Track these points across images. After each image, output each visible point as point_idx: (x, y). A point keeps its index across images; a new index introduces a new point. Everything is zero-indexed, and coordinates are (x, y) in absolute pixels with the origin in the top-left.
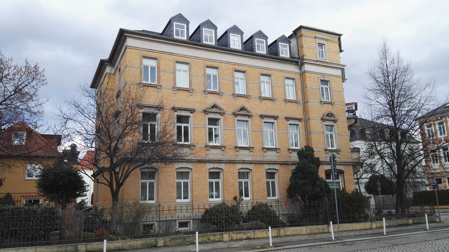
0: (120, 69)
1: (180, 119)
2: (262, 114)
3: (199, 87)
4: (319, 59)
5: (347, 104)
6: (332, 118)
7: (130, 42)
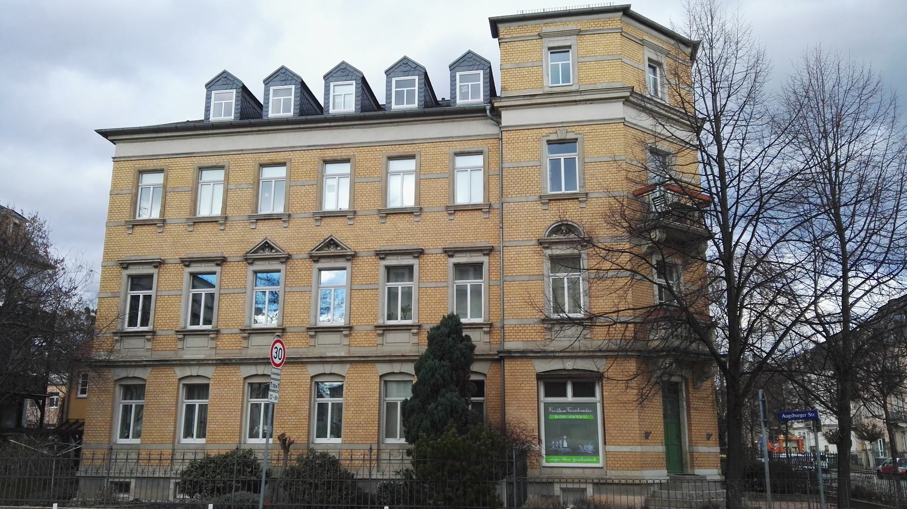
1: (138, 282)
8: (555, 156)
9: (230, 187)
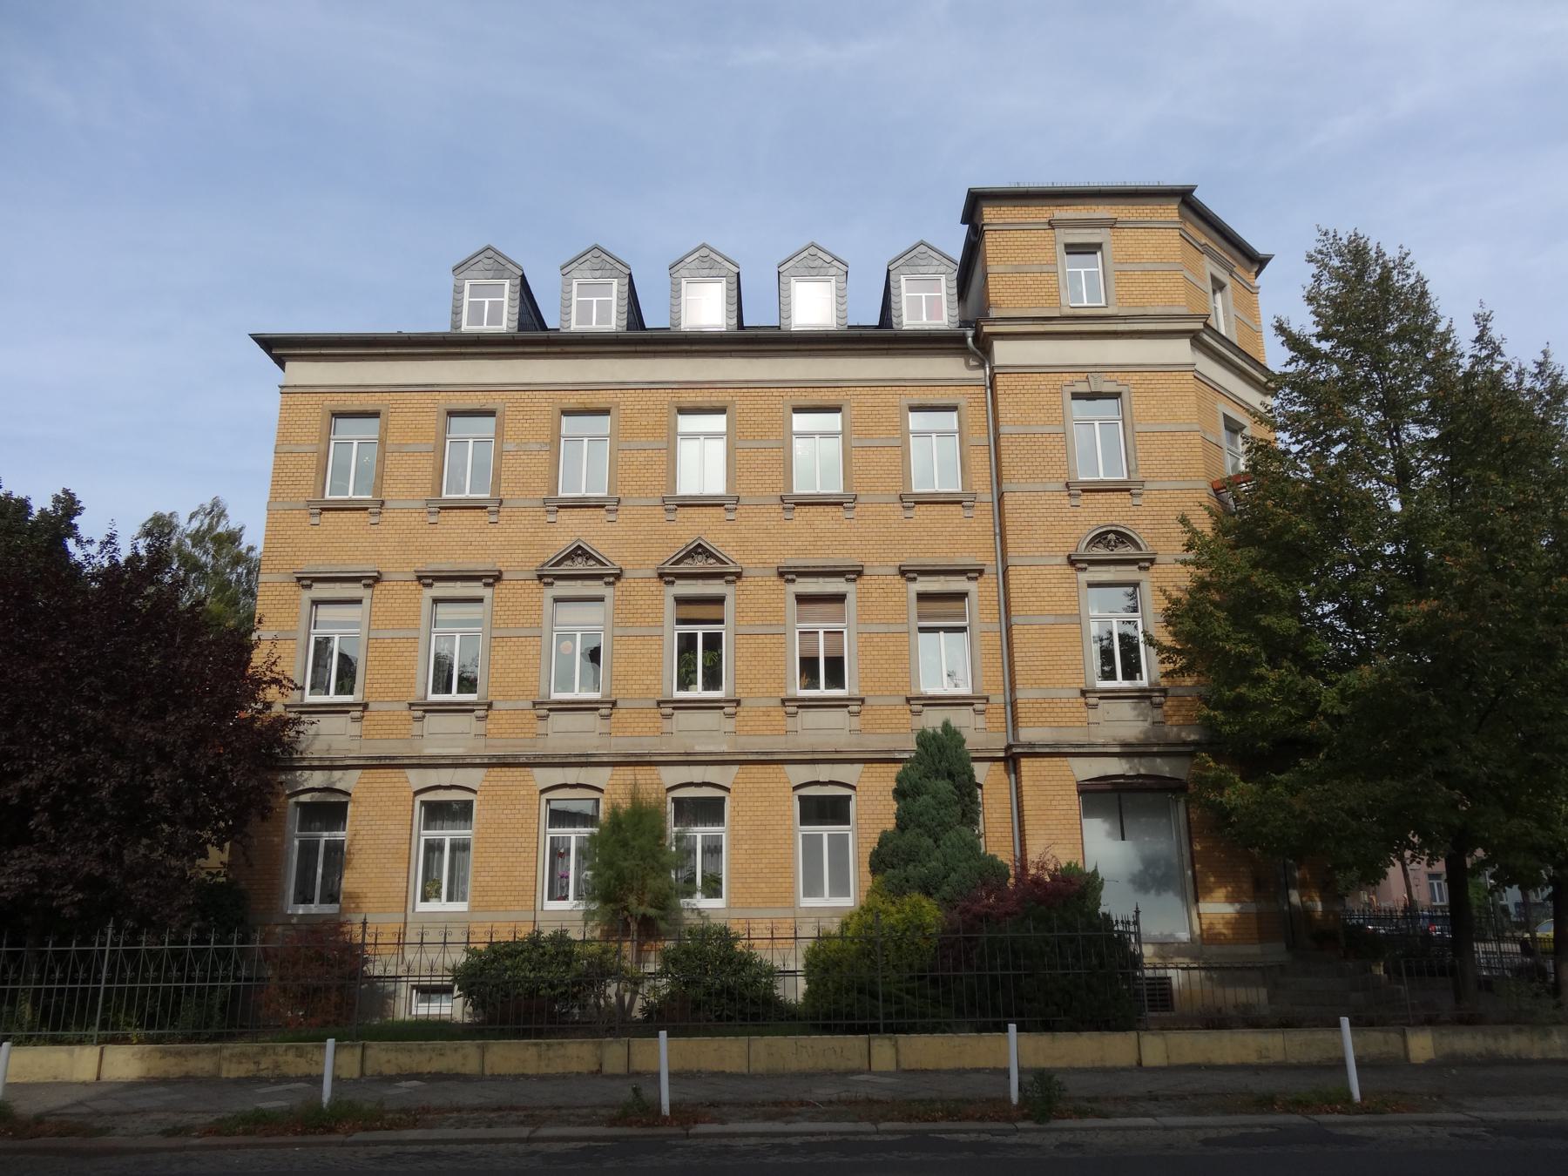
9: (507, 447)
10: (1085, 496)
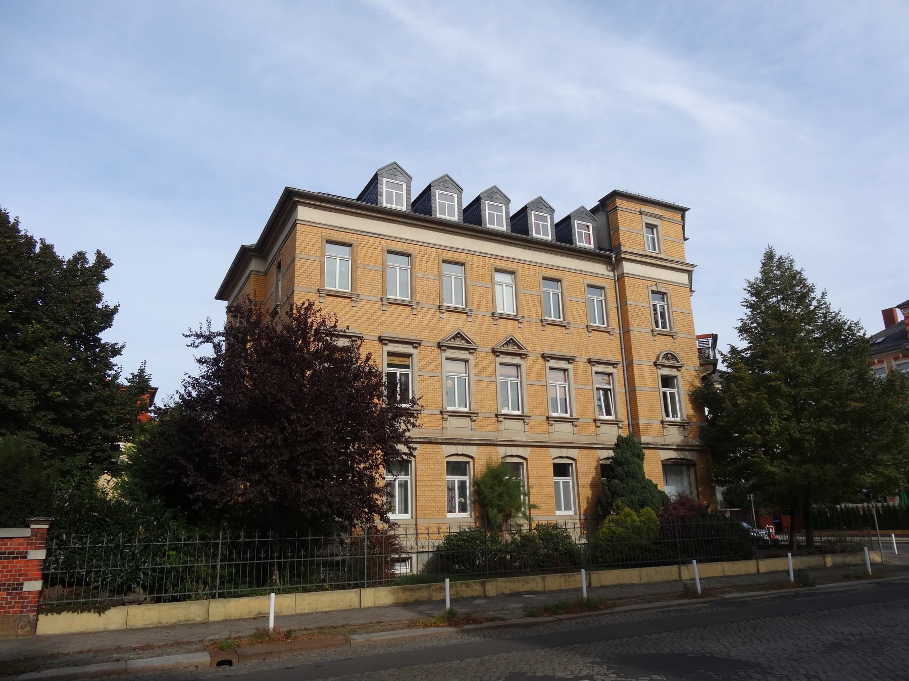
0: (280, 263)
2: (546, 352)
3: (532, 313)
4: (648, 253)
5: (699, 337)
6: (672, 362)
7: (304, 213)
8: (655, 302)
10: (390, 306)
